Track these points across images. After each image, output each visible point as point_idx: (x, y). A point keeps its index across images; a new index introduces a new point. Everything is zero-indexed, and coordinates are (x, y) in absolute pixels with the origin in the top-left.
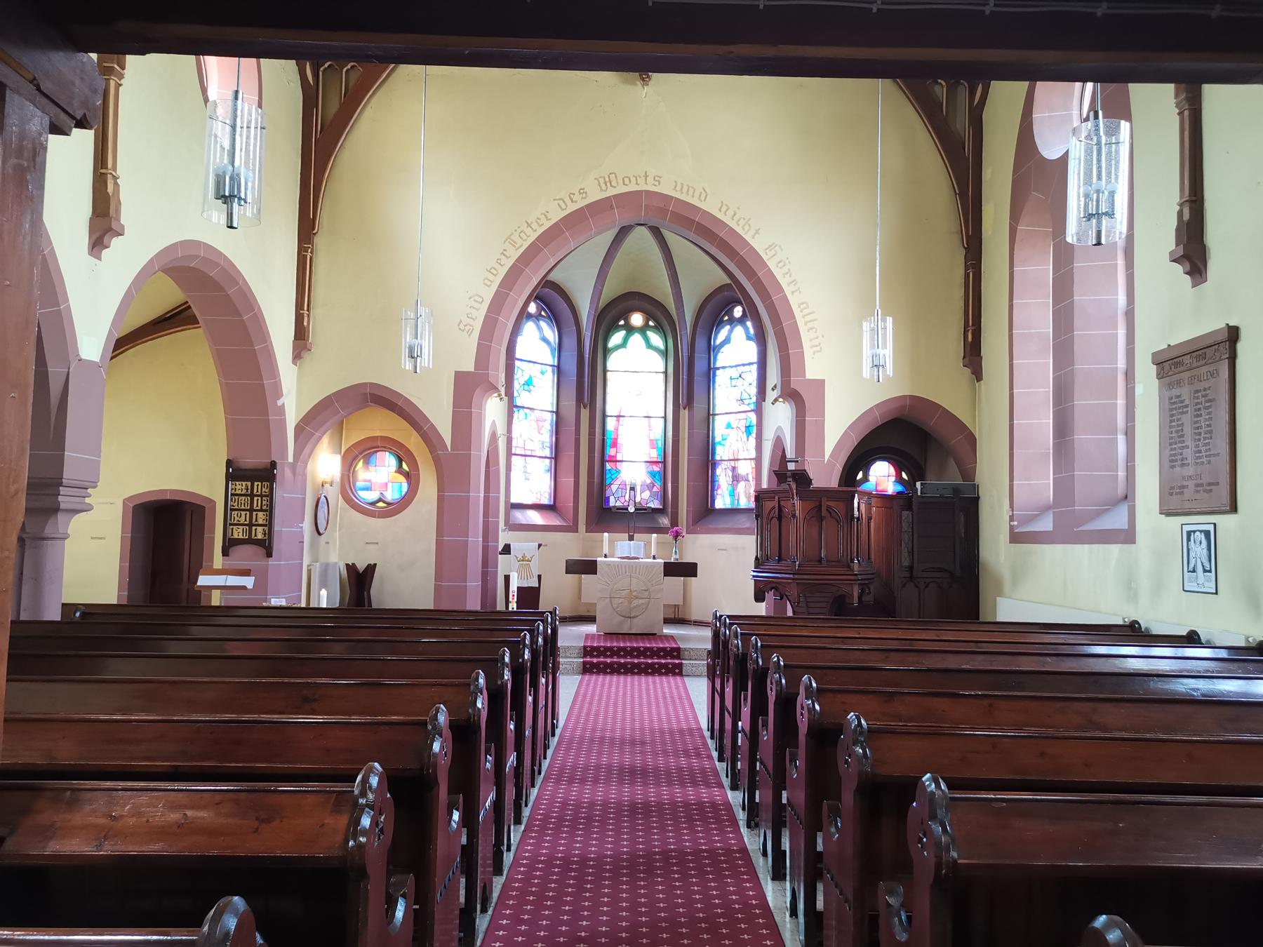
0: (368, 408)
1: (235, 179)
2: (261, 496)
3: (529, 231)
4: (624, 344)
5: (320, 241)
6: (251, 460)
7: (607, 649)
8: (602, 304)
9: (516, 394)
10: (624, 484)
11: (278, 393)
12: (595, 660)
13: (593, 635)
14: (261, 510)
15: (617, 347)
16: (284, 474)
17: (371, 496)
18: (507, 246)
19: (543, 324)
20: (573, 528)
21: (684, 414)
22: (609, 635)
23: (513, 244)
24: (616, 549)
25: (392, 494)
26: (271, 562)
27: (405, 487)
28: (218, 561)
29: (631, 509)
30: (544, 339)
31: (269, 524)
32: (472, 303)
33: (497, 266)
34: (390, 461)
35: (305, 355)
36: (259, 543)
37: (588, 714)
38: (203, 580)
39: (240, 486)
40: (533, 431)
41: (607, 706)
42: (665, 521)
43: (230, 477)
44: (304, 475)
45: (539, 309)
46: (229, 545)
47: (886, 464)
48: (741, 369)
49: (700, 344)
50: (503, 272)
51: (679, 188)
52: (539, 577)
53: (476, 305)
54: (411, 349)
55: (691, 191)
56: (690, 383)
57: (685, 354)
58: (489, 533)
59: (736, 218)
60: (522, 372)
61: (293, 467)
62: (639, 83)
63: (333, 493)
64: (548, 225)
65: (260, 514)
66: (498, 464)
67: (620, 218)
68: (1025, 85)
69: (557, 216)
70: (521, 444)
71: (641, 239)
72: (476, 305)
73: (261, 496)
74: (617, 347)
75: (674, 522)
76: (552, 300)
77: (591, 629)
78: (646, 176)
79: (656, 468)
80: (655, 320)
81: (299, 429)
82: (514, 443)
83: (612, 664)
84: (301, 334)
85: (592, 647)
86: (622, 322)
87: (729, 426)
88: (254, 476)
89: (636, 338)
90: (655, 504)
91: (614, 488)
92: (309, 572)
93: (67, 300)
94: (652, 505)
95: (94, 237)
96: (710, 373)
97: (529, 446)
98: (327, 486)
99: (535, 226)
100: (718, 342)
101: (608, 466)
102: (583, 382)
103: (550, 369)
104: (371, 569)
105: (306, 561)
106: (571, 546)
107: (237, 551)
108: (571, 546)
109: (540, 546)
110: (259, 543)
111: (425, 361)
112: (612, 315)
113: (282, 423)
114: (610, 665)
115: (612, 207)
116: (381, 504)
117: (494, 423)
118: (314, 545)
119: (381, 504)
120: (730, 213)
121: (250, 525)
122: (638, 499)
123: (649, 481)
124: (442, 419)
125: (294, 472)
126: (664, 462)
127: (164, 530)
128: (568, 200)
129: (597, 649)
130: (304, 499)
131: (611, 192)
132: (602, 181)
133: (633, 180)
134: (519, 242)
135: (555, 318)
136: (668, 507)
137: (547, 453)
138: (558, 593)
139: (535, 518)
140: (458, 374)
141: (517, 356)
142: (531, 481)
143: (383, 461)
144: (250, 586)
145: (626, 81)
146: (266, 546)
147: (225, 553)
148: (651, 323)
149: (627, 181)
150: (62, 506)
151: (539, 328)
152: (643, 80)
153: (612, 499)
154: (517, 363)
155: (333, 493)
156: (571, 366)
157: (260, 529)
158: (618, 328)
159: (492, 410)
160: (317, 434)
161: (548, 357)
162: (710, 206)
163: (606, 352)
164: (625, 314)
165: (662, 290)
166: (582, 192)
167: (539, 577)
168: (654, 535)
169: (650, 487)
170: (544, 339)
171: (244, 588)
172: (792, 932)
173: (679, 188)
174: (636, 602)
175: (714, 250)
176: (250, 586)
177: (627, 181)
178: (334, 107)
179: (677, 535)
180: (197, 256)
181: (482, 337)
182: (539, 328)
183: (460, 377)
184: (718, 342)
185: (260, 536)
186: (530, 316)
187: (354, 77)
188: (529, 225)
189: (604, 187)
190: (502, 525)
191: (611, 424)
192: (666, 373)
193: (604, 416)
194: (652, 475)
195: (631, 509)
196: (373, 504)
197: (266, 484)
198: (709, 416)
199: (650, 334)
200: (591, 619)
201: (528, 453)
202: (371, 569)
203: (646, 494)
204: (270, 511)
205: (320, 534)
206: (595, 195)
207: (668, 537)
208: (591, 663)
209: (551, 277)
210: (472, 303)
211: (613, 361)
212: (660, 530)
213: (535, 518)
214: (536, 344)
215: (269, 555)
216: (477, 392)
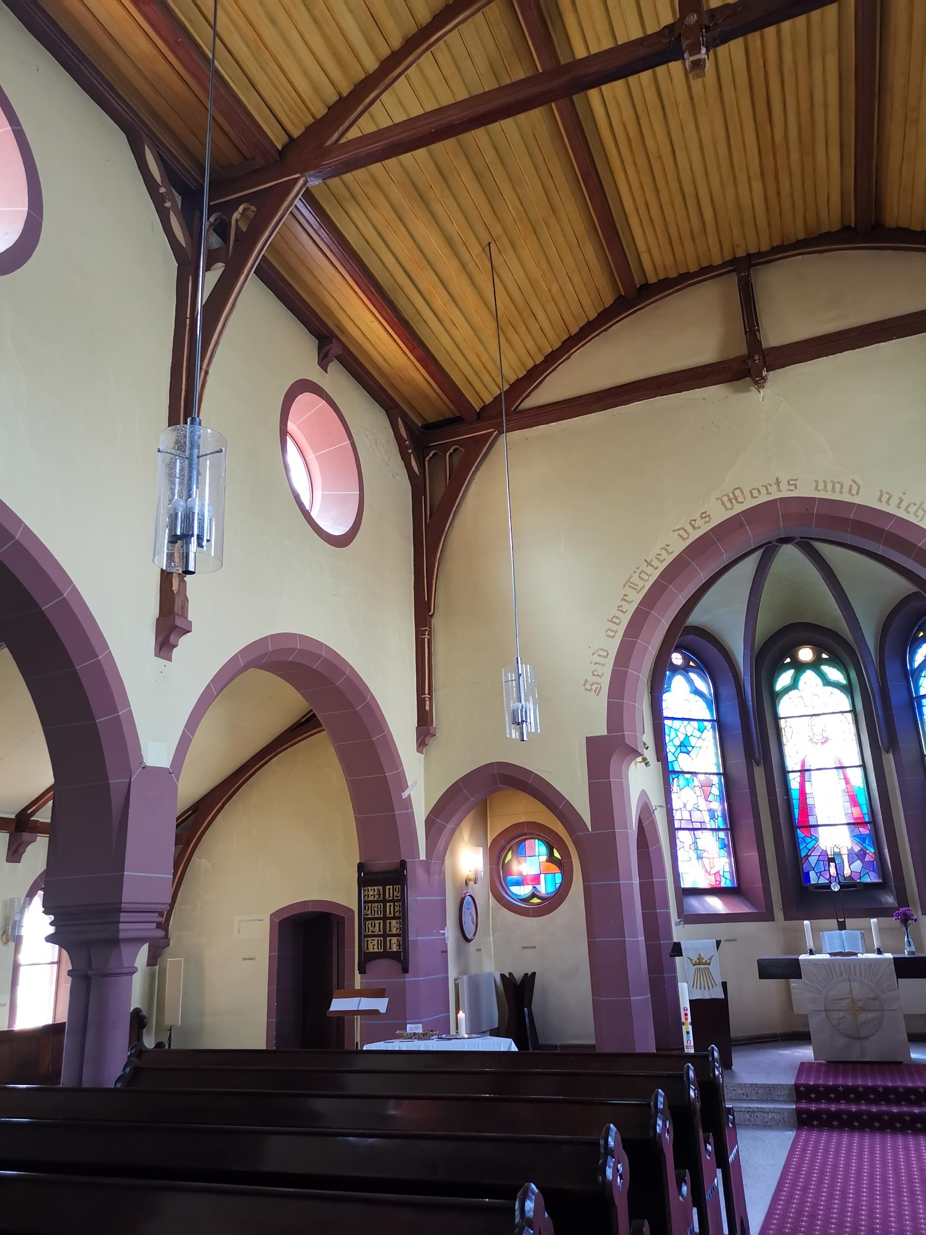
0: (493, 790)
1: (188, 518)
2: (393, 901)
3: (649, 570)
4: (794, 686)
5: (438, 623)
6: (382, 863)
7: (829, 1089)
8: (758, 643)
9: (671, 758)
10: (824, 853)
11: (403, 785)
12: (813, 1107)
13: (810, 1065)
14: (394, 918)
15: (787, 690)
16: (417, 875)
17: (524, 891)
18: (627, 590)
19: (693, 676)
20: (766, 915)
21: (889, 760)
22: (836, 1066)
23: (634, 587)
24: (825, 943)
25: (546, 887)
26: (409, 978)
27: (559, 878)
28: (358, 981)
29: (836, 888)
30: (697, 692)
31: (403, 934)
32: (596, 659)
33: (619, 614)
34: (539, 849)
35: (432, 743)
36: (394, 956)
37: (799, 1213)
38: (338, 1005)
39: (372, 892)
40: (697, 799)
41: (831, 1196)
42: (890, 899)
43: (363, 883)
44: (442, 873)
45: (686, 659)
46: (367, 959)
49: (892, 670)
50: (626, 619)
51: (821, 487)
52: (724, 985)
53: (602, 660)
54: (514, 713)
55: (838, 486)
57: (875, 686)
58: (655, 926)
59: (903, 505)
60: (674, 734)
61: (426, 864)
62: (753, 389)
63: (481, 892)
64: (669, 559)
65: (394, 922)
66: (657, 841)
67: (752, 536)
69: (678, 547)
70: (686, 816)
71: (790, 557)
72: (602, 660)
73: (393, 901)
74: (787, 690)
75: (903, 899)
76: (695, 646)
77: (806, 1053)
78: (778, 482)
79: (864, 831)
80: (828, 651)
81: (430, 822)
82: (677, 815)
83: (839, 1113)
84: (425, 720)
85: (807, 1086)
86: (788, 660)
88: (386, 878)
89: (809, 676)
90: (871, 878)
91: (813, 860)
92: (457, 986)
93: (128, 704)
94: (867, 880)
95: (160, 639)
97: (697, 816)
98: (471, 883)
99: (655, 563)
100: (916, 665)
102: (751, 734)
103: (708, 725)
104: (534, 974)
105: (452, 974)
106: (765, 940)
107: (372, 966)
108: (765, 940)
109: (718, 943)
110: (394, 956)
111: (532, 725)
112: (774, 653)
113: (410, 818)
114: (837, 1115)
115: (742, 525)
116: (535, 900)
117: (643, 793)
118: (460, 954)
119: (535, 900)
120: (894, 501)
121: (385, 936)
122: (847, 872)
123: (857, 849)
124: (576, 792)
125: (428, 872)
126: (873, 822)
127: (308, 944)
128: (689, 528)
129: (815, 1088)
130: (444, 902)
131: (738, 509)
132: (725, 499)
133: (763, 490)
134: (641, 583)
135: (706, 668)
136: (890, 878)
137: (720, 823)
138: (753, 1001)
139: (716, 904)
140: (589, 740)
141: (666, 713)
142: (703, 862)
143: (533, 848)
144: (383, 1010)
145: (737, 391)
146: (401, 960)
147: (362, 971)
148: (824, 656)
149: (755, 493)
150: (122, 935)
151: (690, 682)
152: (756, 383)
153: (812, 875)
154: (666, 722)
155: (481, 892)
156: (733, 718)
157: (394, 940)
159: (639, 779)
160: (450, 826)
161: (702, 710)
162: (866, 498)
163: (775, 697)
164: (791, 652)
165: (828, 609)
166: (705, 516)
167: (724, 985)
168: (873, 921)
169: (861, 855)
170: (697, 692)
171: (376, 1012)
173: (821, 487)
174: (863, 1016)
175: (881, 550)
176: (383, 1010)
177: (755, 493)
178: (440, 491)
179: (906, 919)
180: (294, 650)
181: (611, 695)
182: (690, 682)
183: (592, 742)
184: (916, 665)
185: (395, 948)
186: (675, 669)
187: (457, 458)
188: (649, 564)
189: (729, 505)
190: (674, 917)
191: (794, 782)
192: (854, 711)
193: (785, 773)
194: (861, 839)
195: (836, 888)
196: (526, 900)
197: (397, 887)
199: (825, 668)
200: (800, 1037)
201: (698, 826)
202: (534, 974)
203: (858, 865)
204: (403, 917)
205: (468, 941)
206: (719, 516)
207: (893, 922)
208: (808, 1112)
209: (696, 618)
210: (596, 659)
211: (785, 707)
212: (881, 912)
213: (716, 904)
214: (686, 698)
215: (405, 970)
216: (614, 759)
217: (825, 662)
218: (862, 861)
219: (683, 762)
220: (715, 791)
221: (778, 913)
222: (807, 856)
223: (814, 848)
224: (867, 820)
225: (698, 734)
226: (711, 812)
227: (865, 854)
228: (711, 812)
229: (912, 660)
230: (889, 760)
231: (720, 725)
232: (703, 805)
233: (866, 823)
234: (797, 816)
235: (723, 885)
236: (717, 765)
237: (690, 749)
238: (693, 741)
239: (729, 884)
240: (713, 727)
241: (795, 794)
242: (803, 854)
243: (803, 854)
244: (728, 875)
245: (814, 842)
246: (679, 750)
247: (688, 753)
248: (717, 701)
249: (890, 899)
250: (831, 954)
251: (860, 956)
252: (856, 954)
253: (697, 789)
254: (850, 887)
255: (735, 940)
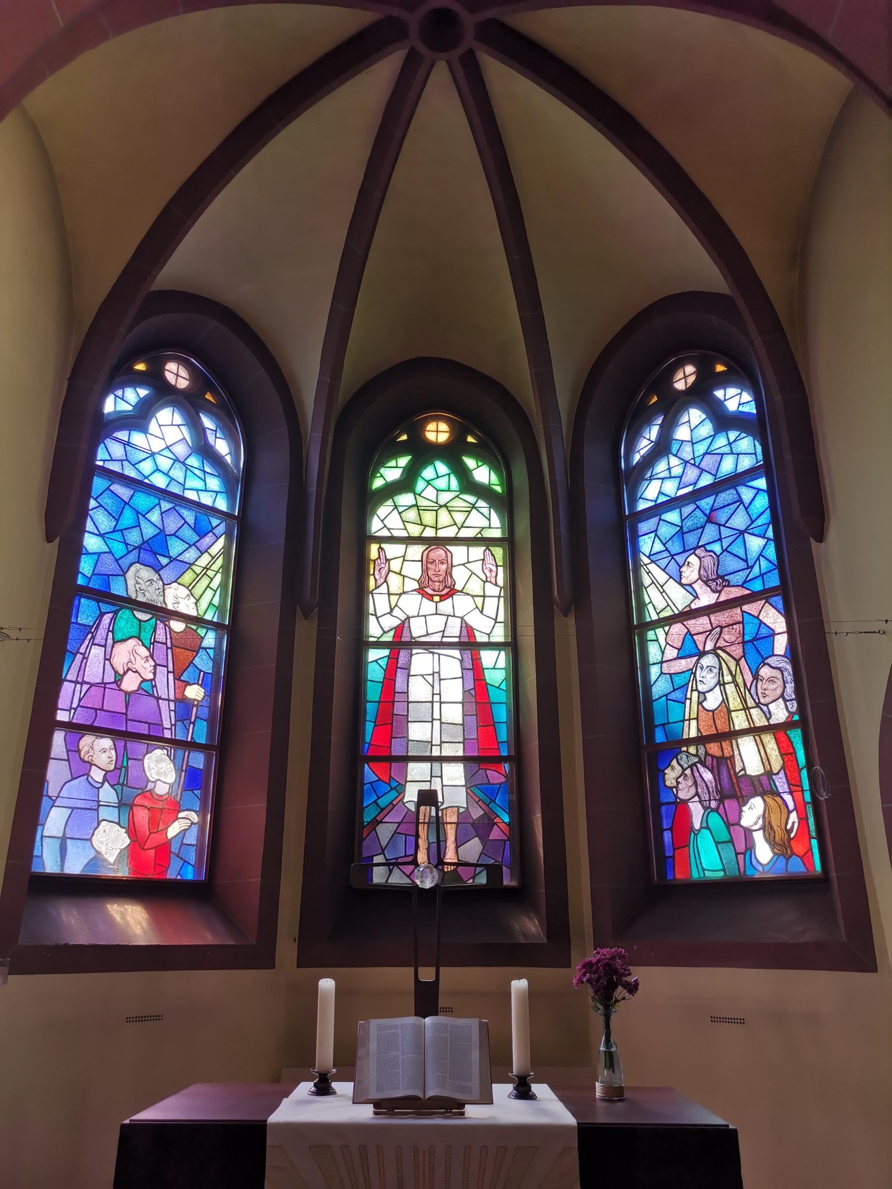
4: (406, 483)
20: (257, 954)
21: (567, 628)
47: (303, 1083)
48: (706, 503)
49: (594, 458)
56: (573, 563)
68: (766, 587)
76: (234, 375)
87: (691, 650)
89: (437, 472)
91: (385, 832)
96: (624, 528)
101: (369, 774)
102: (302, 560)
112: (380, 415)
123: (477, 813)
126: (517, 758)
137: (200, 733)
139: (132, 921)
151: (198, 430)
156: (273, 516)
158: (397, 450)
163: (367, 501)
164: (411, 419)
169: (482, 828)
172: (53, 2)
182: (198, 430)
192: (509, 542)
193: (360, 643)
198: (632, 630)
211: (385, 519)
212: (517, 956)
213: (132, 921)
217: (471, 450)
218: (484, 839)
219: (396, 871)
220: (204, 663)
221: (286, 949)
222: (376, 822)
223: (392, 806)
224: (504, 753)
225: (188, 534)
226: (183, 706)
227: (492, 824)
228: (183, 706)
229: (631, 449)
230: (567, 628)
231: (243, 528)
232: (165, 686)
233: (501, 759)
234: (368, 739)
235: (172, 874)
236: (220, 609)
237: (164, 561)
238: (175, 547)
239: (189, 874)
240: (228, 534)
241: (373, 692)
242: (367, 819)
243: (367, 819)
244: (192, 857)
245: (394, 794)
246: (133, 557)
247: (157, 569)
248: (244, 483)
249: (530, 927)
250: (382, 1106)
251: (474, 1113)
252: (455, 1106)
253: (160, 650)
254: (452, 896)
255: (158, 1018)
